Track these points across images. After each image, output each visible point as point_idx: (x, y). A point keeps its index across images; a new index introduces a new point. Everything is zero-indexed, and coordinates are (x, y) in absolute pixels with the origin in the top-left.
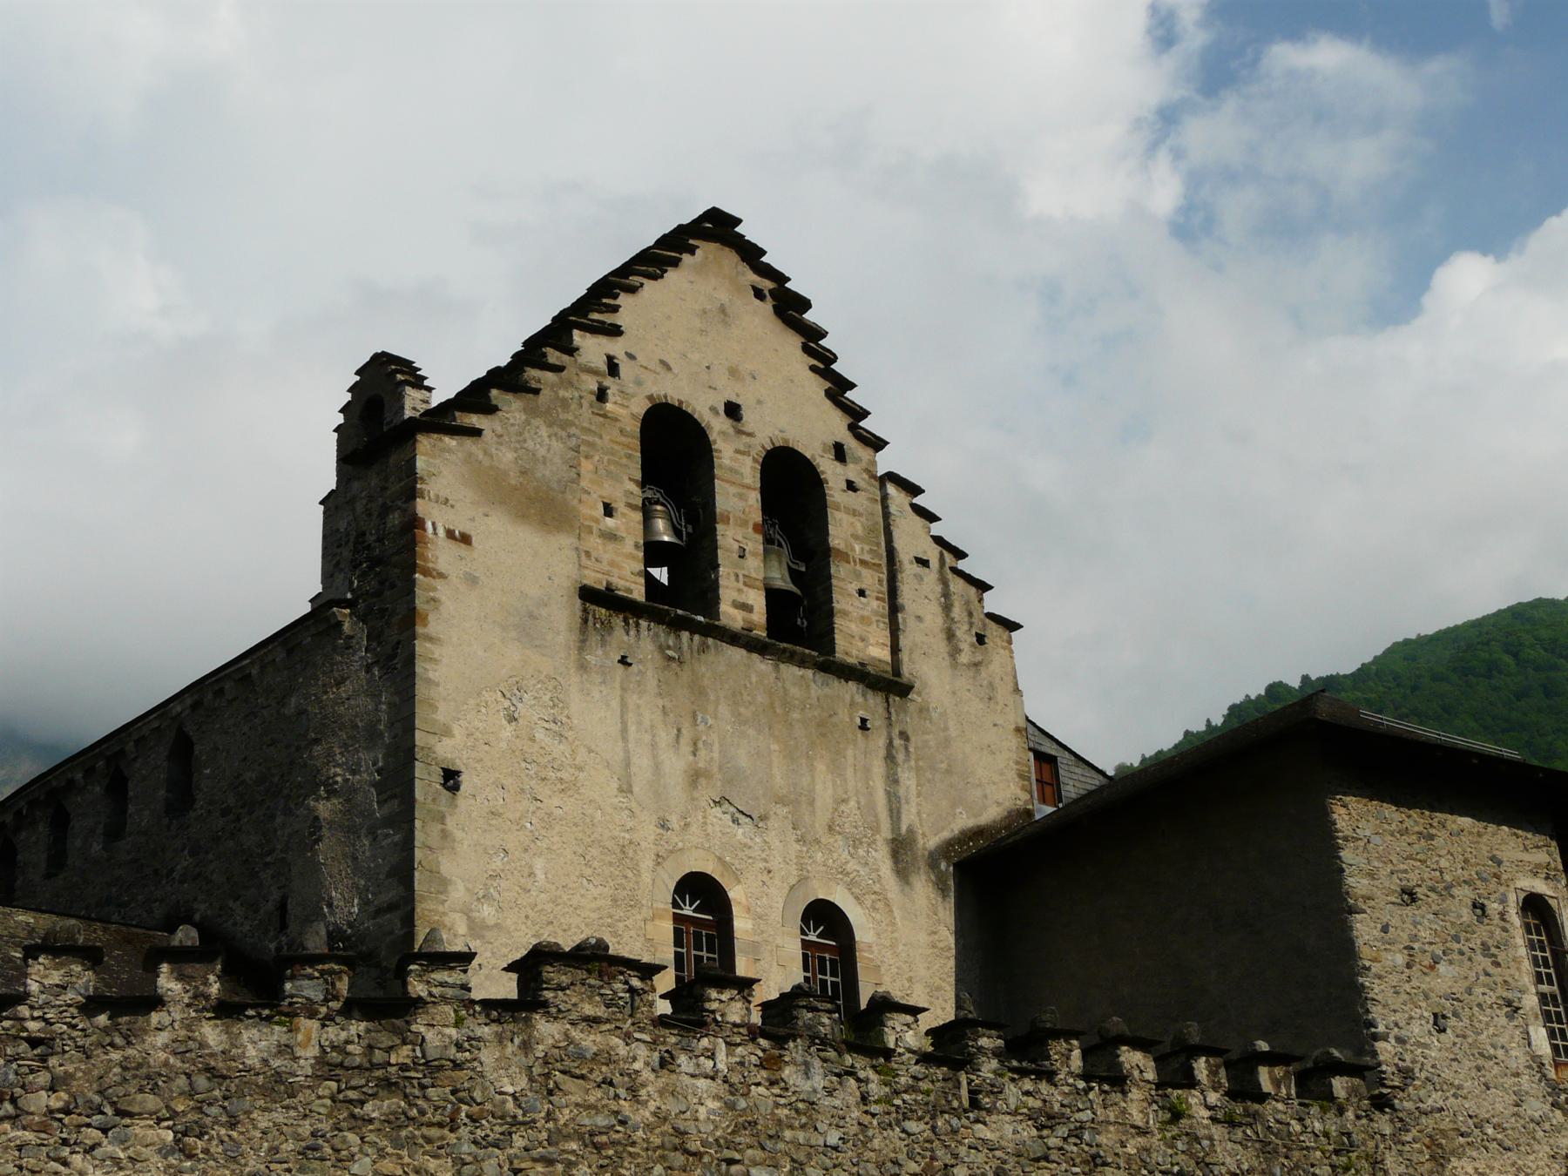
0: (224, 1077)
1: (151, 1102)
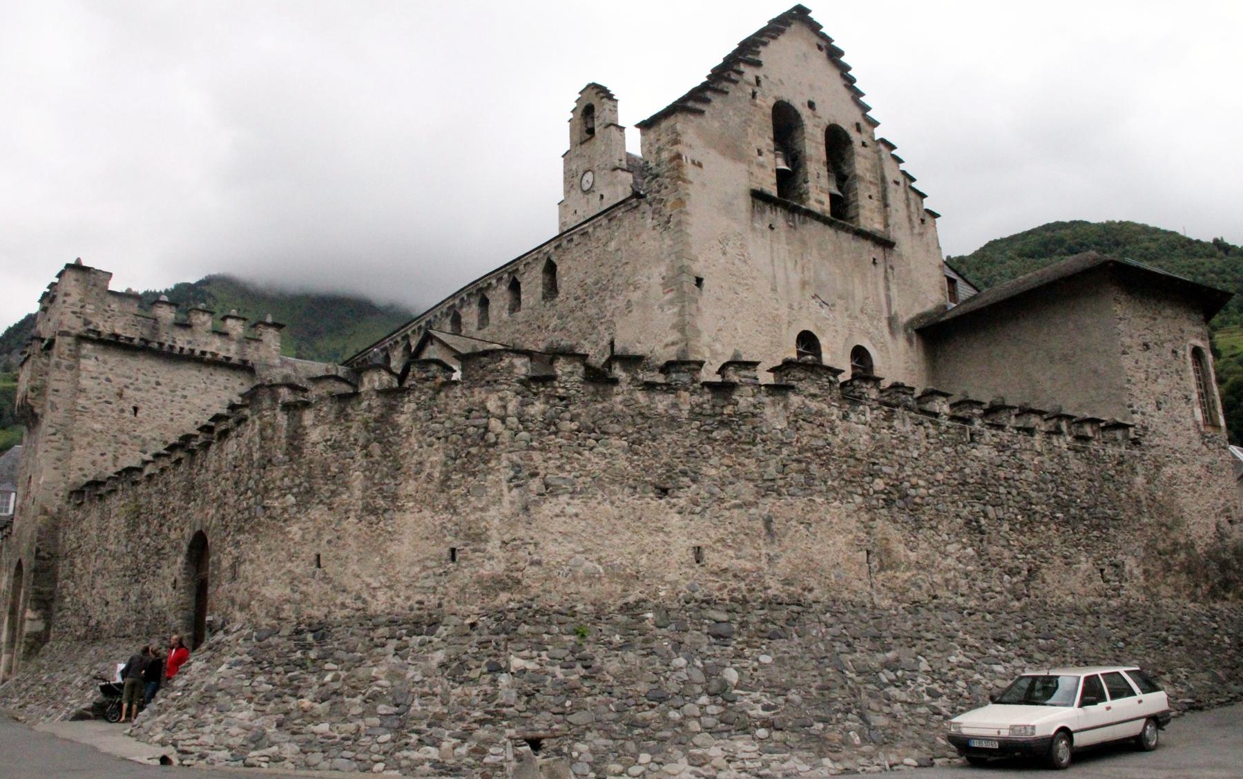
0: (648, 418)
1: (617, 428)
